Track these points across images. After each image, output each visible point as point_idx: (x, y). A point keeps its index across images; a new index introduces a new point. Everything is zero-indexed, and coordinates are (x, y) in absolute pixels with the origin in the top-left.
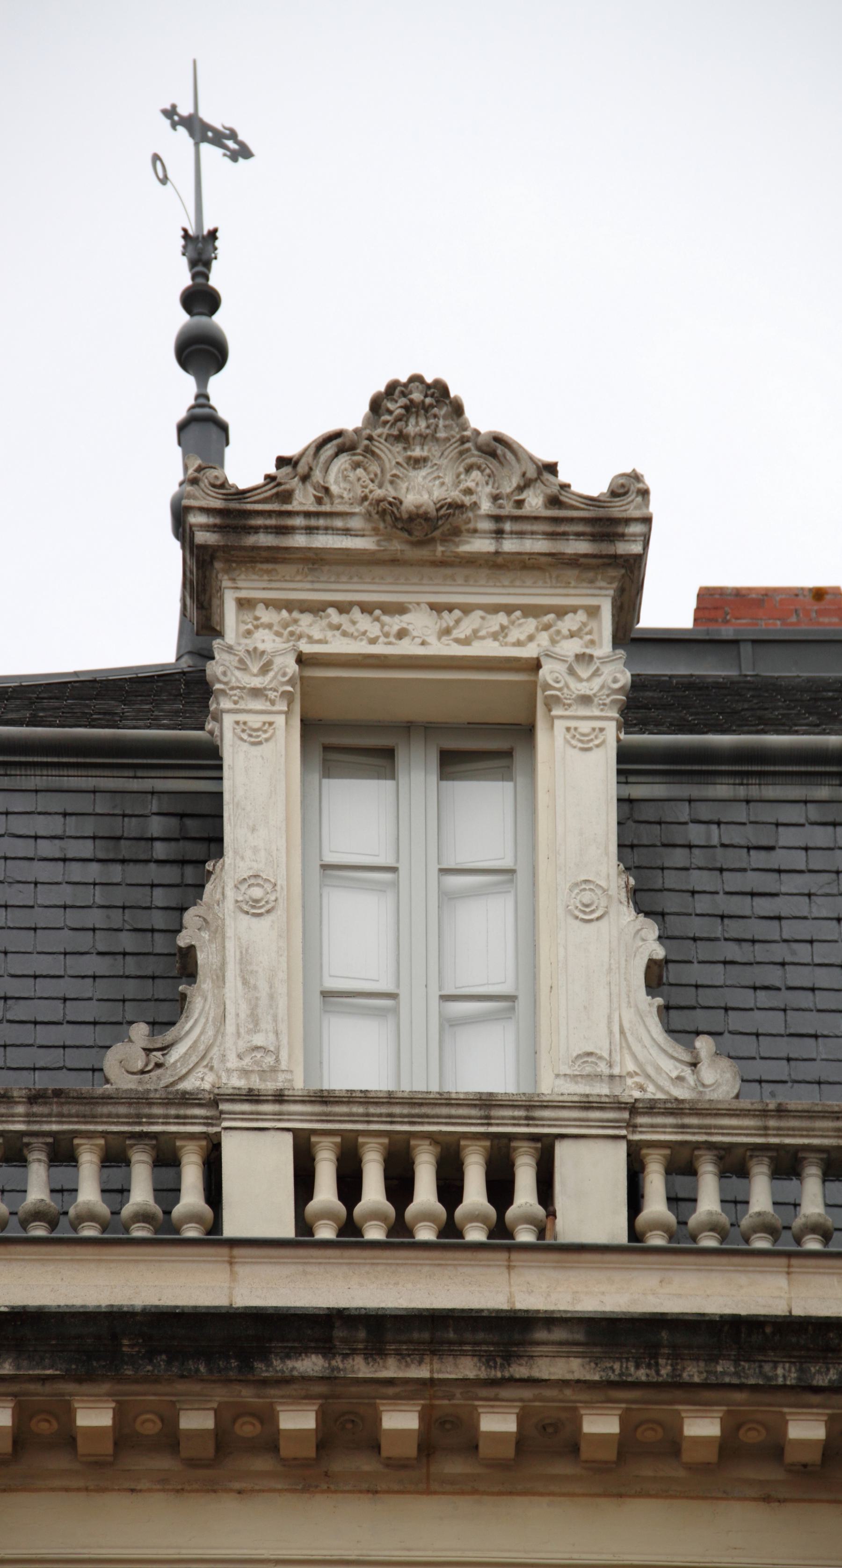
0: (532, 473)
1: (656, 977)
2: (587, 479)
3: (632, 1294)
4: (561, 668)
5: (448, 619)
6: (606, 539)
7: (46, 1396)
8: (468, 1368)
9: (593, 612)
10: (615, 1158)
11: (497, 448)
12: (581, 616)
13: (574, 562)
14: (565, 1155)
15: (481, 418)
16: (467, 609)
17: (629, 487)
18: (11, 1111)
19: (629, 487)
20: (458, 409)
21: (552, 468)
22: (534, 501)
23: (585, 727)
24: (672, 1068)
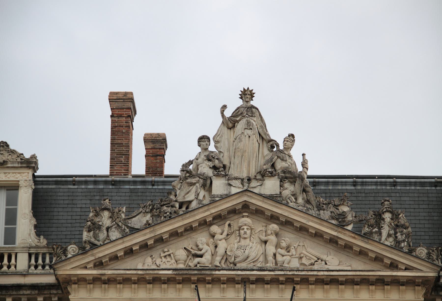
0: (19, 155)
1: (36, 227)
2: (27, 156)
3: (108, 229)
4: (22, 182)
5: (6, 174)
6: (31, 164)
7: (270, 271)
8: (37, 292)
9: (28, 173)
10: (26, 255)
11: (13, 152)
12: (26, 174)
13: (24, 167)
14: (18, 255)
15: (12, 147)
16: (9, 173)
17: (34, 157)
18: (19, 293)
19: (34, 157)
20: (8, 146)
21: (22, 154)
22: (19, 160)
23: (26, 190)
24: (36, 240)
